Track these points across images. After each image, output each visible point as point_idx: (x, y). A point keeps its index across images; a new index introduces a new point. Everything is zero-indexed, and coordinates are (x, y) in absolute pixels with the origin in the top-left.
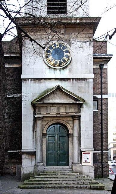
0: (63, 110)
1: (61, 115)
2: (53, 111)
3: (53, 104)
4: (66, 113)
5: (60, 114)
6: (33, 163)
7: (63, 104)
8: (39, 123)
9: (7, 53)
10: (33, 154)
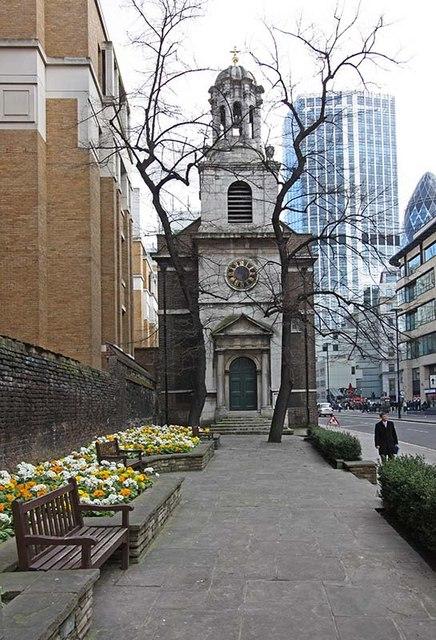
2: (237, 345)
3: (236, 336)
6: (214, 407)
7: (249, 336)
8: (221, 358)
10: (214, 396)
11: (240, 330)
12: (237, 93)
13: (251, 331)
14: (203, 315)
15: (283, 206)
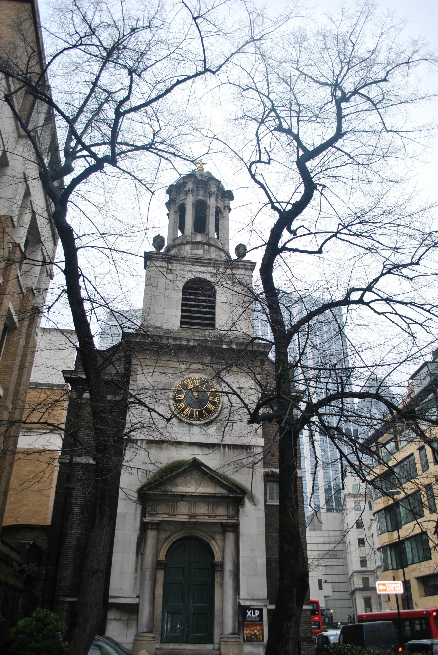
0: (202, 509)
1: (199, 520)
3: (183, 497)
4: (210, 517)
5: (198, 517)
6: (132, 632)
8: (151, 535)
10: (131, 610)
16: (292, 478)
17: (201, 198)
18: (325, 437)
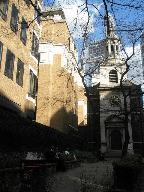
0: (118, 125)
3: (113, 122)
6: (106, 148)
7: (117, 122)
8: (108, 130)
9: (91, 93)
10: (105, 144)
11: (115, 120)
12: (112, 42)
13: (119, 120)
14: (101, 115)
15: (123, 80)
16: (118, 101)
17: (112, 44)
18: (119, 94)
